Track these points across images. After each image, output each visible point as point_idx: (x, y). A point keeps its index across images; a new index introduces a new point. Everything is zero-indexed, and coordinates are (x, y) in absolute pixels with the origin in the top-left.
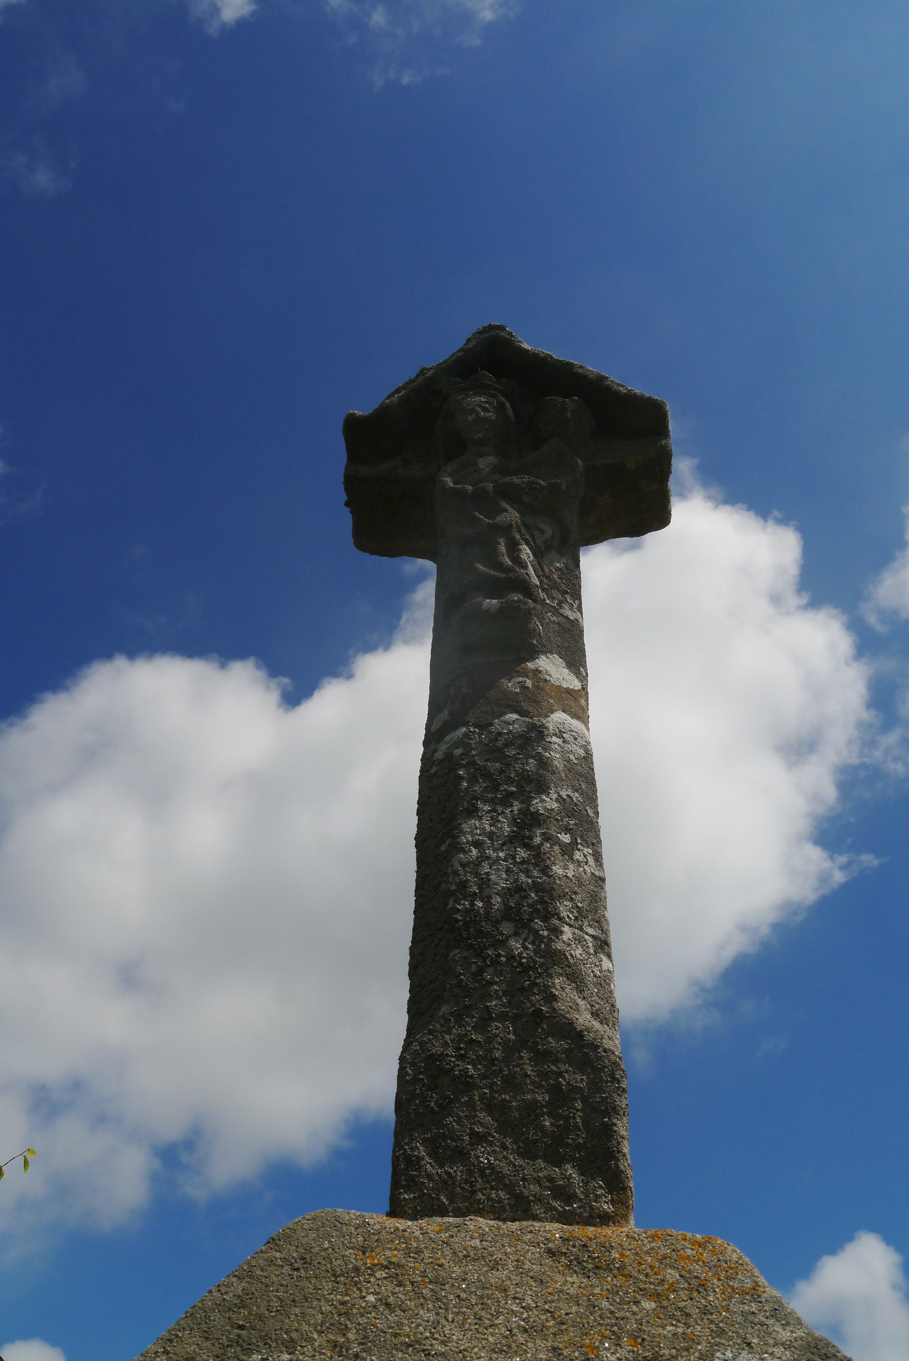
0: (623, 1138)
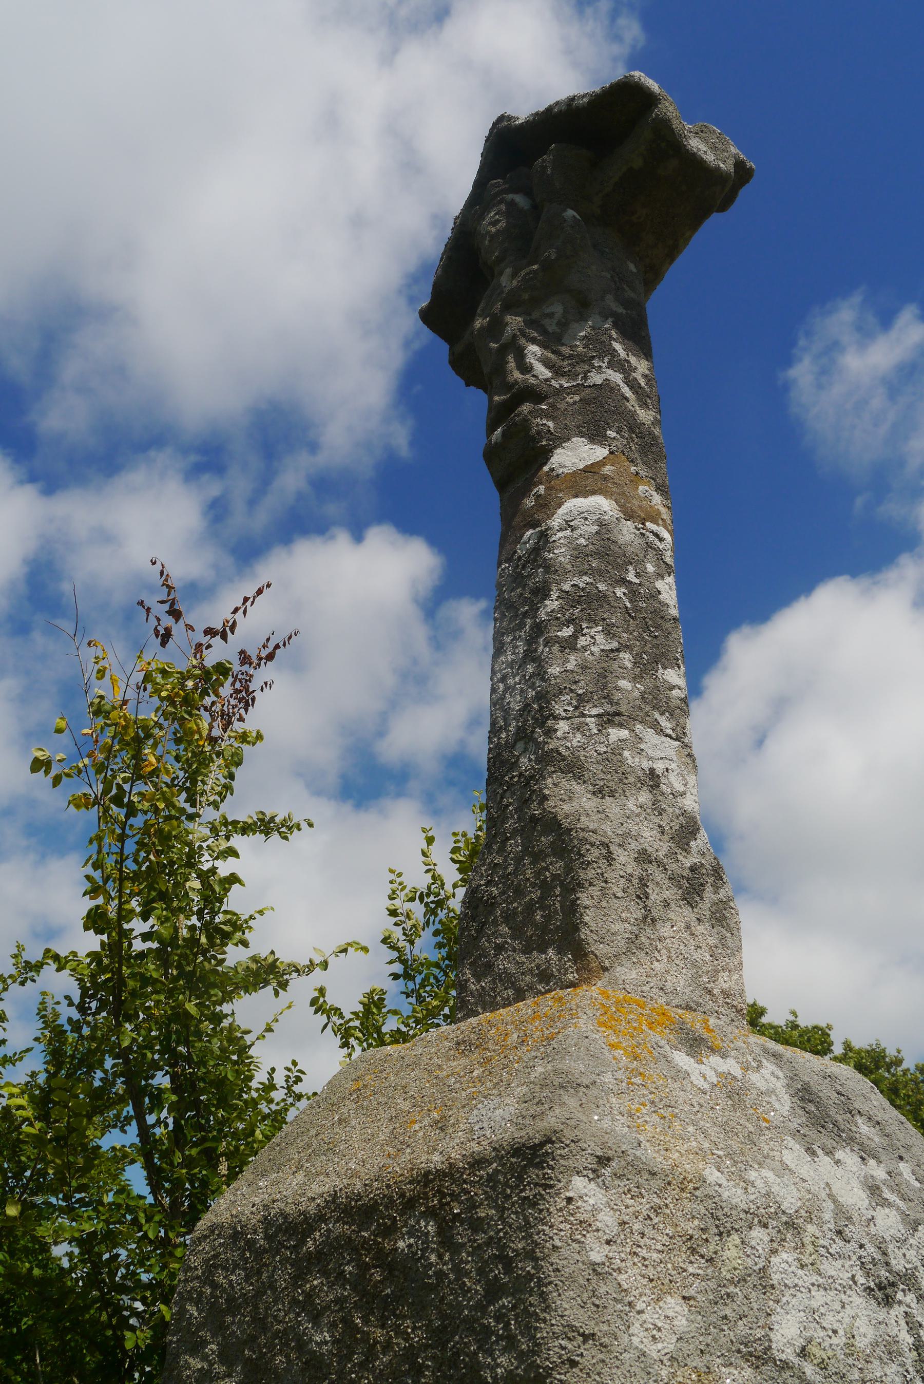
0: (586, 908)
